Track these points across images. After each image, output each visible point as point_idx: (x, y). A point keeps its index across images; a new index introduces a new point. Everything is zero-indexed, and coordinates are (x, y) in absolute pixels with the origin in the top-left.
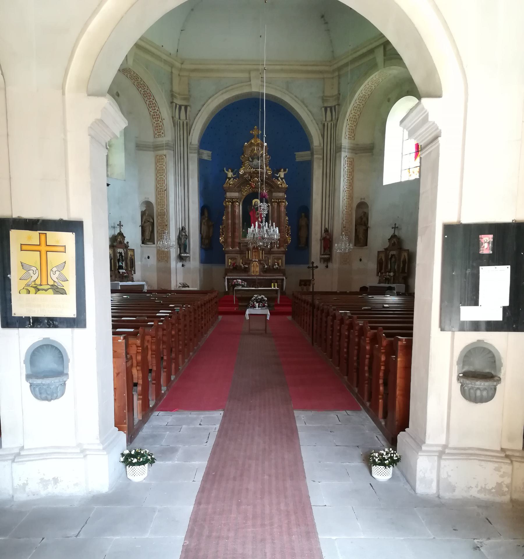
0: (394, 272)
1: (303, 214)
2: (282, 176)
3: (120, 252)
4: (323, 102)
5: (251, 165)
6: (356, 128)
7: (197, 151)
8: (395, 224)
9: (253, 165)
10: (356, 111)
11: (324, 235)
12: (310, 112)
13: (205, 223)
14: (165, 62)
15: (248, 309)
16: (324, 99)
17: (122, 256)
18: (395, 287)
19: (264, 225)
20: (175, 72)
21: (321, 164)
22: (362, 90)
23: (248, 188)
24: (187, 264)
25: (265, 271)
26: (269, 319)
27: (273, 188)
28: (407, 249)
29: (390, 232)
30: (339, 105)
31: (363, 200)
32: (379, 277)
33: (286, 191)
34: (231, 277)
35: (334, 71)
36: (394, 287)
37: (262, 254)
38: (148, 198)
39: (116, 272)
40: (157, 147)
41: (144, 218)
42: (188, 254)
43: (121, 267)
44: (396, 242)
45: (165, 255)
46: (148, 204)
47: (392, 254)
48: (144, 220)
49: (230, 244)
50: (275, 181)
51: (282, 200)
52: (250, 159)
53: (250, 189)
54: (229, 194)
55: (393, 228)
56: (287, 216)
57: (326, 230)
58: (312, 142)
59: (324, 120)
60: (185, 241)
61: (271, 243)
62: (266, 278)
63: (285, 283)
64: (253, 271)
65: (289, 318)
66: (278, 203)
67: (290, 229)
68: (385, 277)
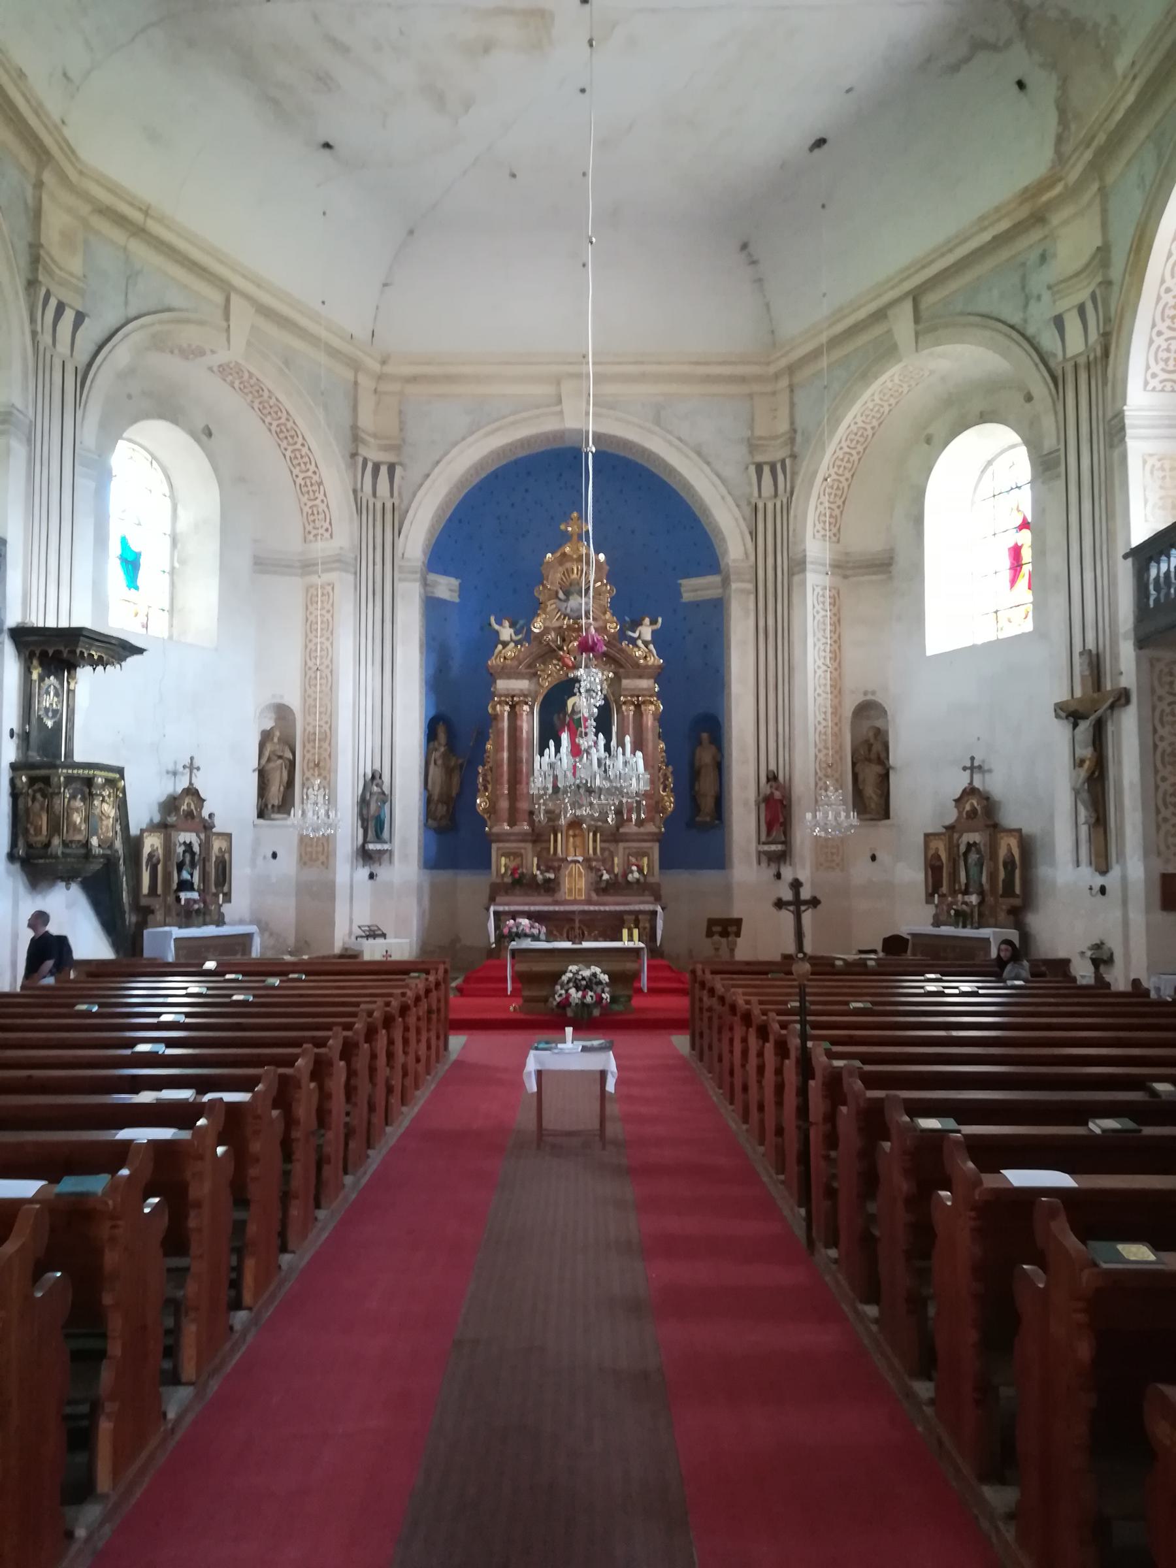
0: (978, 894)
1: (705, 736)
2: (648, 637)
3: (188, 842)
4: (751, 453)
5: (563, 609)
6: (842, 512)
7: (418, 576)
8: (972, 759)
9: (568, 610)
10: (842, 469)
11: (766, 789)
12: (718, 476)
13: (439, 762)
14: (333, 352)
15: (532, 1053)
16: (753, 446)
17: (193, 854)
18: (991, 940)
19: (591, 743)
20: (366, 382)
21: (752, 606)
22: (853, 417)
23: (556, 668)
24: (383, 872)
25: (603, 889)
26: (613, 1091)
27: (621, 666)
28: (1014, 825)
29: (962, 781)
30: (794, 456)
31: (870, 697)
32: (933, 906)
33: (659, 675)
34: (507, 908)
35: (777, 376)
36: (989, 939)
37: (595, 841)
38: (282, 697)
39: (171, 899)
40: (308, 566)
41: (269, 749)
42: (386, 843)
43: (185, 886)
44: (979, 808)
45: (320, 849)
46: (282, 713)
47: (968, 843)
48: (267, 754)
49: (505, 815)
50: (627, 649)
51: (648, 698)
52: (561, 595)
53: (559, 670)
54: (502, 685)
55: (965, 769)
56: (663, 741)
57: (770, 777)
58: (726, 551)
59: (756, 493)
60: (380, 808)
61: (619, 812)
62: (607, 908)
63: (660, 923)
64: (570, 890)
65: (681, 1042)
66: (638, 706)
67: (672, 773)
68: (954, 907)
